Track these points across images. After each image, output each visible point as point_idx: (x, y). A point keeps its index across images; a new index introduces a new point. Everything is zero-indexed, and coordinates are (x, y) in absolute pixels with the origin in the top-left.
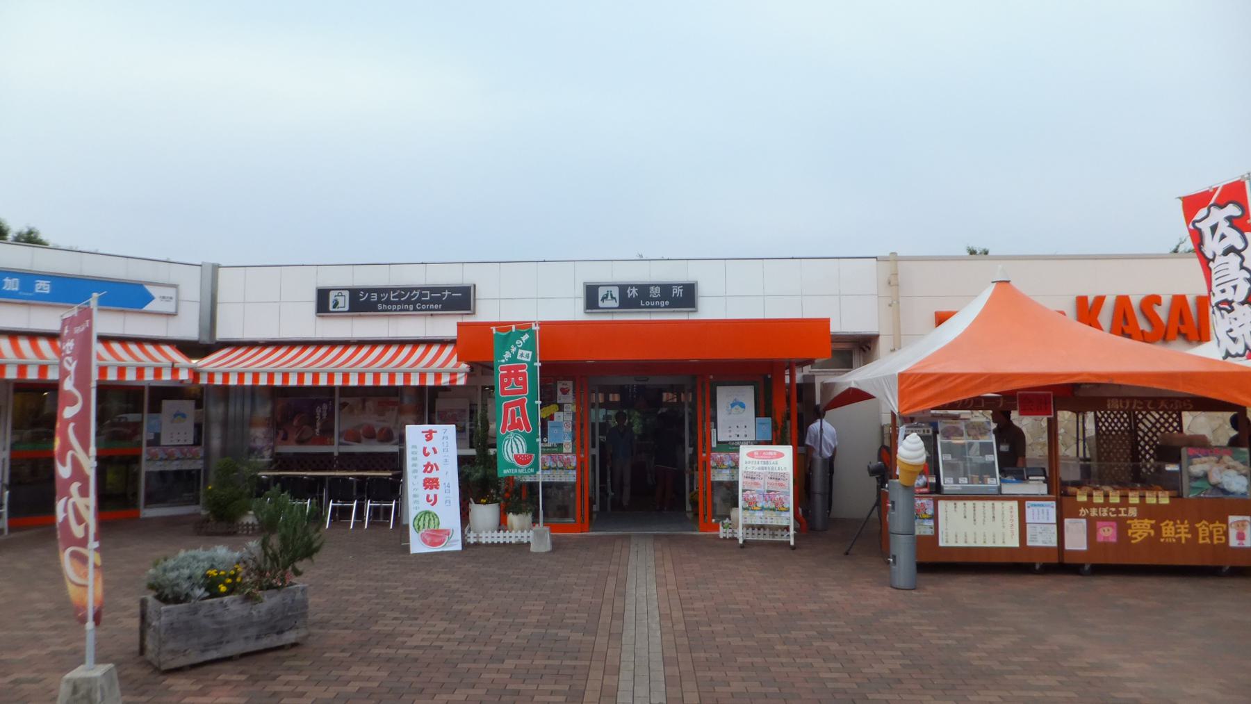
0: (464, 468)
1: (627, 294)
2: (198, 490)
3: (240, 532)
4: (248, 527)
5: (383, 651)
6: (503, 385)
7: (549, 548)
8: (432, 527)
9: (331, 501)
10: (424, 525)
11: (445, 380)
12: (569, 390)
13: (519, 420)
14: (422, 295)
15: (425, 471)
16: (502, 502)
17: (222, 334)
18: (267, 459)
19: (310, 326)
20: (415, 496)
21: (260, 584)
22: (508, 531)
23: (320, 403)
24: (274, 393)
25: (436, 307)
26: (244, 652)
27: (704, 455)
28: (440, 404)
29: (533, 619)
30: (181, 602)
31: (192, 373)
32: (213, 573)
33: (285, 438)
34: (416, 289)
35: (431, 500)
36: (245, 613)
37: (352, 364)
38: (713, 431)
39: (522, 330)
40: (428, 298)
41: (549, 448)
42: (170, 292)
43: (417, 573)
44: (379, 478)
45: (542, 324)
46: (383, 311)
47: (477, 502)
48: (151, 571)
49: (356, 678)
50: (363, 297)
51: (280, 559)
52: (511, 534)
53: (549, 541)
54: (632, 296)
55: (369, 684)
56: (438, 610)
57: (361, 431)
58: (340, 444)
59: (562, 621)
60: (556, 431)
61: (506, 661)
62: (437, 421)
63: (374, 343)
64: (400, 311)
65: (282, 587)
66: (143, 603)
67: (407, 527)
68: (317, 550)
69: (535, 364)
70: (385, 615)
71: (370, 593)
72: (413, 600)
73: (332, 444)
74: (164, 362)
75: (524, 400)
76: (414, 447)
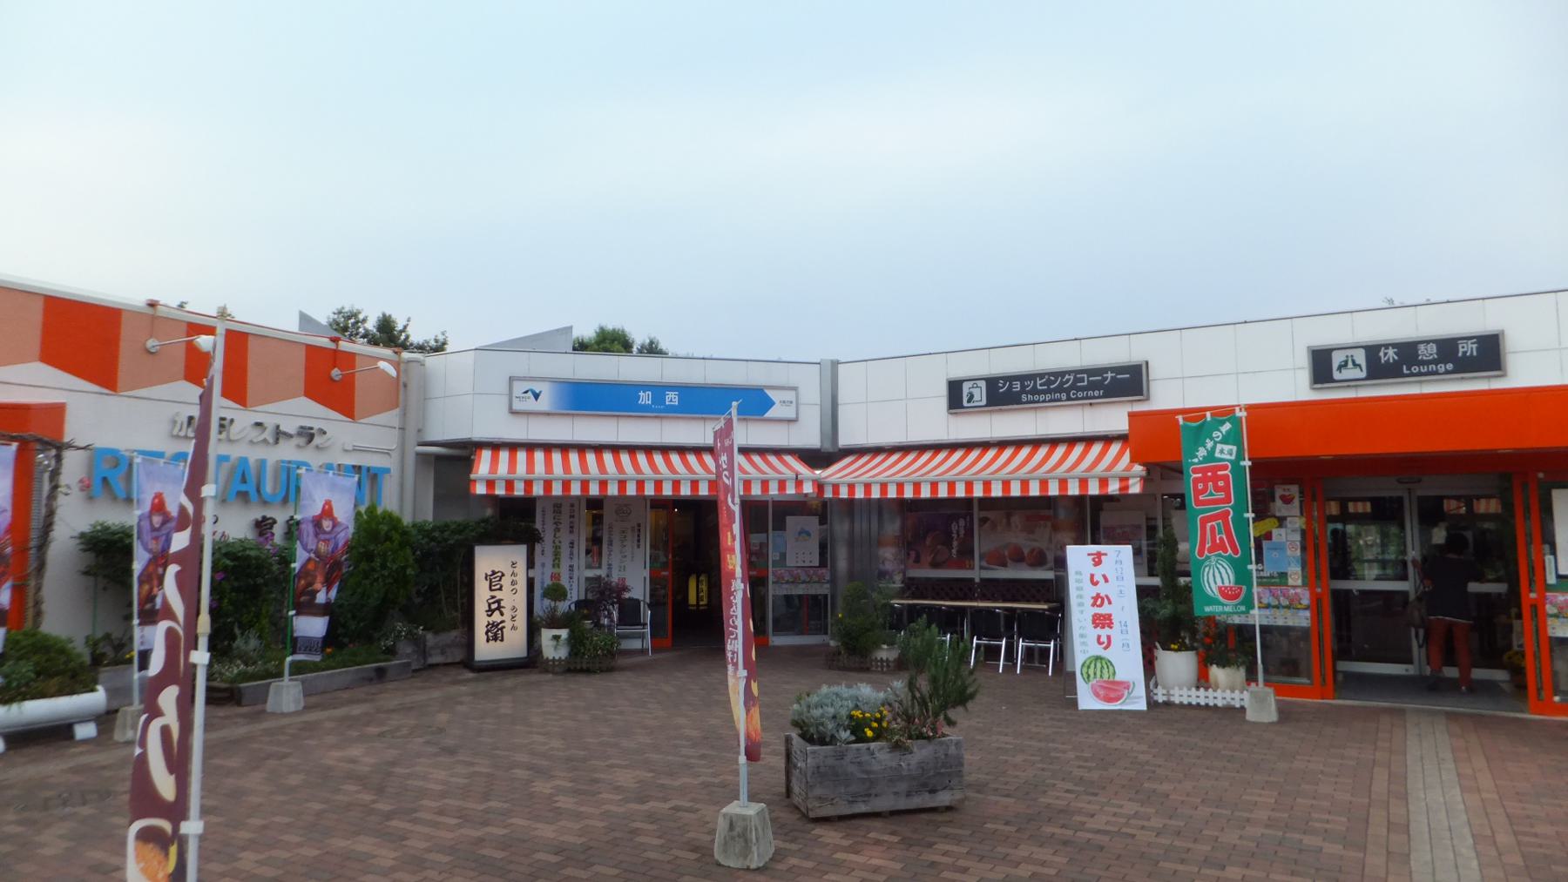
0: (1146, 602)
1: (1380, 358)
2: (826, 617)
3: (874, 669)
4: (882, 664)
5: (1058, 831)
6: (1198, 492)
7: (1274, 717)
8: (1106, 677)
9: (975, 638)
10: (1095, 674)
11: (1113, 488)
12: (1293, 498)
13: (1221, 539)
14: (1077, 380)
15: (1093, 605)
16: (1201, 650)
17: (844, 441)
18: (898, 585)
19: (939, 425)
20: (1082, 636)
21: (909, 731)
22: (1210, 690)
23: (955, 518)
24: (908, 508)
25: (1096, 393)
26: (921, 807)
27: (1533, 595)
28: (1106, 519)
29: (1263, 815)
30: (826, 744)
31: (816, 486)
32: (857, 713)
33: (917, 560)
34: (1069, 372)
35: (1103, 643)
36: (894, 764)
37: (1050, 467)
38: (1549, 559)
39: (1221, 418)
40: (1086, 383)
41: (1264, 577)
42: (790, 395)
43: (1091, 736)
44: (1031, 612)
45: (1250, 408)
46: (1028, 402)
47: (1166, 648)
48: (796, 706)
49: (1029, 860)
50: (1002, 388)
51: (929, 704)
52: (1207, 694)
53: (1273, 707)
54: (1389, 359)
55: (1046, 871)
56: (1123, 786)
57: (1006, 553)
58: (982, 568)
59: (1307, 823)
60: (1275, 554)
61: (1227, 868)
62: (1102, 540)
63: (1018, 444)
64: (1049, 401)
65: (934, 737)
66: (788, 740)
67: (1074, 674)
68: (972, 696)
69: (1242, 463)
70: (1055, 785)
71: (1032, 755)
72: (1090, 769)
73: (972, 568)
74: (788, 474)
75: (1228, 512)
76: (1079, 573)
